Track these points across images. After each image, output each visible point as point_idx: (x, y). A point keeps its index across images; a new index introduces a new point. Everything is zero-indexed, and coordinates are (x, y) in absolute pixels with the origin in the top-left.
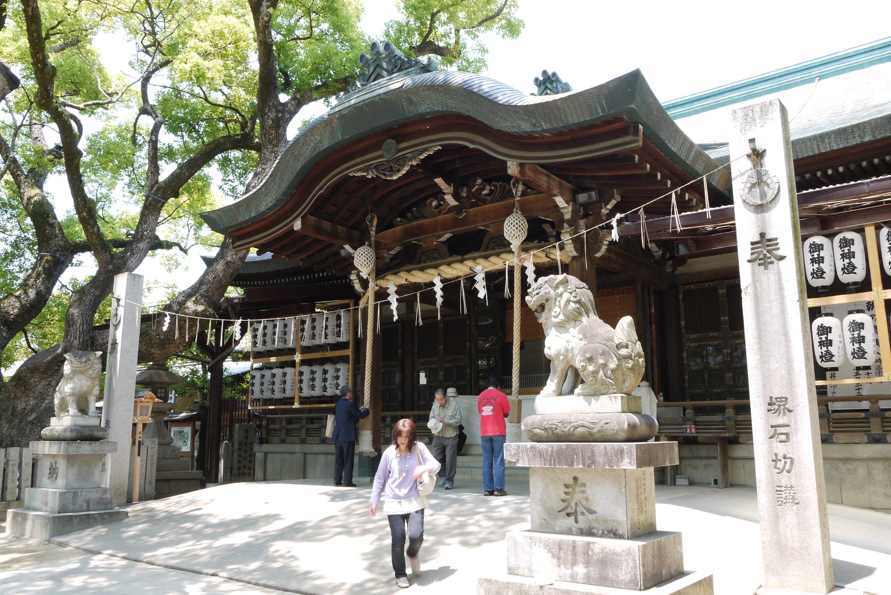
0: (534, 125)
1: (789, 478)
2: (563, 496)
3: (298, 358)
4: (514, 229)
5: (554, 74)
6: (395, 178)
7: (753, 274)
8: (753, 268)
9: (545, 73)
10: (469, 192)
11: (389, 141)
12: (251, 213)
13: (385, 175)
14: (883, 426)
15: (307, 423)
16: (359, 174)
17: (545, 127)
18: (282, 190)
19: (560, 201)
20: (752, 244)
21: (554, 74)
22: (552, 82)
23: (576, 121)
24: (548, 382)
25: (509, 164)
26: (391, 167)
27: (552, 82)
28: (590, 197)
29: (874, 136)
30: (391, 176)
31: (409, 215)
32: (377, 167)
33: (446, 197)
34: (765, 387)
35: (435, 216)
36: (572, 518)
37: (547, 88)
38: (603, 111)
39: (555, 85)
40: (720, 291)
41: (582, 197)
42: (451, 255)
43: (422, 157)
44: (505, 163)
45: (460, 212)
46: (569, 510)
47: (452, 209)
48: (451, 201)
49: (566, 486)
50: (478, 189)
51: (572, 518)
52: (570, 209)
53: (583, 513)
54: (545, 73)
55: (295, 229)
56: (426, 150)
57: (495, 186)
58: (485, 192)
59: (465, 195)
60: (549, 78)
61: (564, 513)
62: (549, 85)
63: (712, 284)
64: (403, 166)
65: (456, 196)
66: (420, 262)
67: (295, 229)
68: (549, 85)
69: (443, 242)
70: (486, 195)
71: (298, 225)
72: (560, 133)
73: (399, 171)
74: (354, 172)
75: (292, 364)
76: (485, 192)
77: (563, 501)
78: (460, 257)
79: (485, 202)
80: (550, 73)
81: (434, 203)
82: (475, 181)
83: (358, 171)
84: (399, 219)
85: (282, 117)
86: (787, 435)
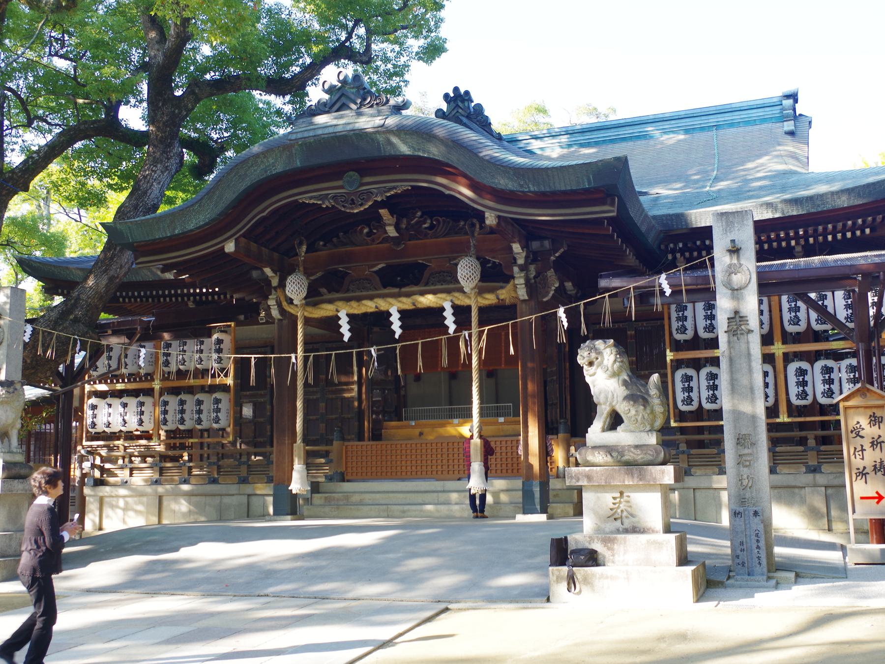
0: (521, 186)
1: (752, 493)
2: (612, 506)
3: (157, 385)
4: (467, 272)
5: (467, 93)
6: (355, 211)
7: (729, 342)
8: (729, 337)
9: (456, 89)
10: (408, 224)
11: (351, 173)
12: (174, 229)
13: (344, 206)
14: (774, 460)
15: (161, 461)
16: (312, 201)
17: (532, 189)
18: (218, 210)
19: (516, 247)
20: (728, 319)
21: (467, 93)
22: (463, 101)
23: (563, 188)
24: (595, 422)
25: (487, 215)
26: (352, 200)
27: (463, 101)
28: (542, 246)
29: (783, 213)
30: (352, 208)
31: (335, 240)
32: (335, 197)
33: (388, 228)
34: (735, 427)
35: (367, 244)
36: (619, 521)
37: (457, 106)
38: (589, 182)
39: (466, 104)
40: (629, 332)
41: (535, 245)
42: (385, 287)
43: (388, 194)
44: (484, 212)
45: (399, 244)
46: (616, 516)
47: (388, 239)
48: (392, 231)
49: (614, 498)
50: (417, 223)
51: (619, 521)
52: (524, 254)
53: (627, 517)
54: (456, 89)
55: (227, 250)
56: (395, 188)
57: (438, 221)
58: (426, 226)
59: (404, 226)
60: (460, 95)
61: (612, 518)
62: (460, 104)
63: (621, 325)
64: (367, 201)
65: (397, 227)
66: (348, 291)
67: (227, 250)
68: (460, 104)
69: (376, 272)
70: (426, 228)
71: (230, 247)
72: (543, 194)
73: (361, 205)
74: (306, 198)
75: (149, 392)
76: (426, 226)
77: (611, 509)
78: (396, 290)
79: (426, 236)
80: (462, 91)
81: (366, 231)
82: (416, 213)
83: (311, 198)
84: (321, 243)
85: (180, 113)
86: (749, 461)
